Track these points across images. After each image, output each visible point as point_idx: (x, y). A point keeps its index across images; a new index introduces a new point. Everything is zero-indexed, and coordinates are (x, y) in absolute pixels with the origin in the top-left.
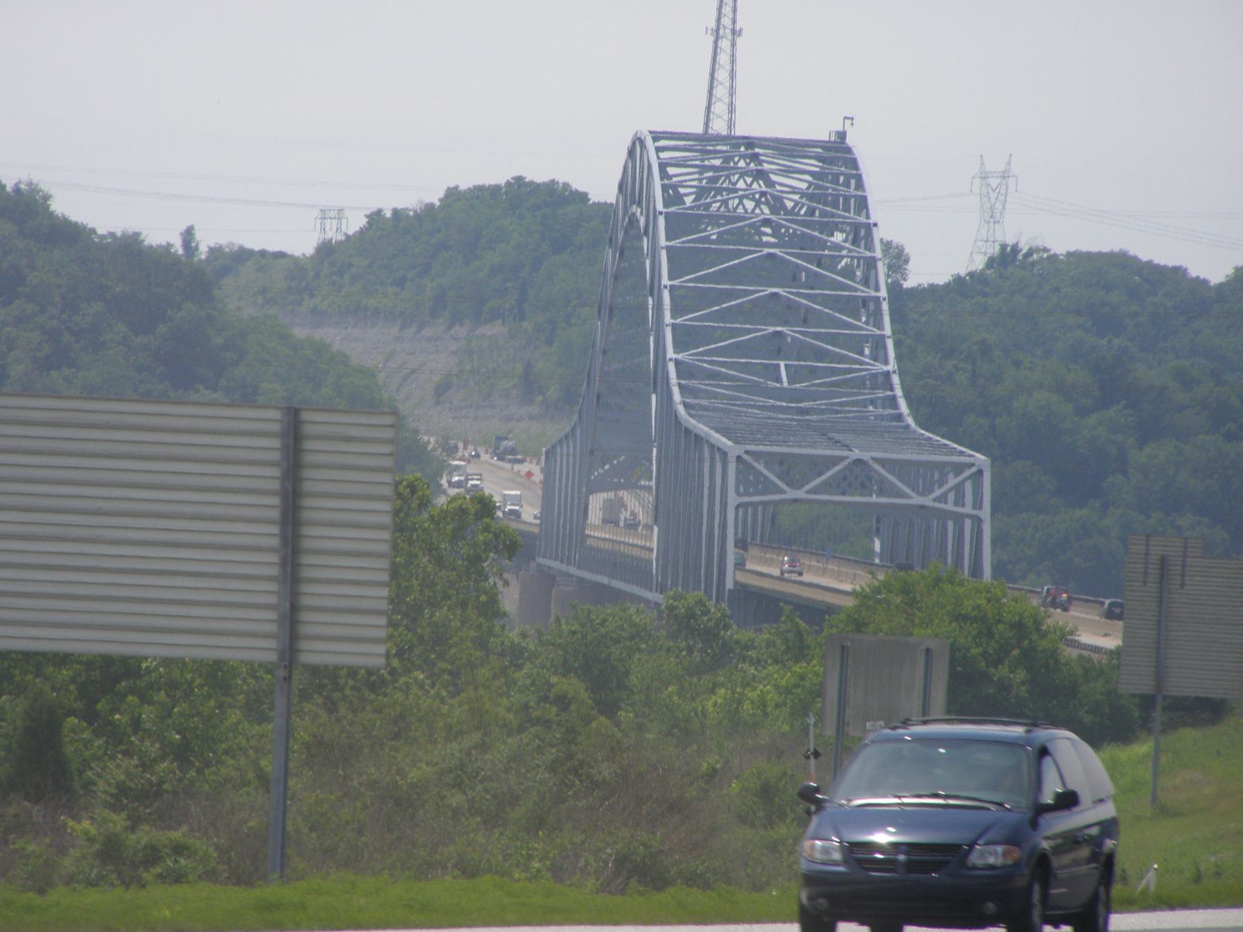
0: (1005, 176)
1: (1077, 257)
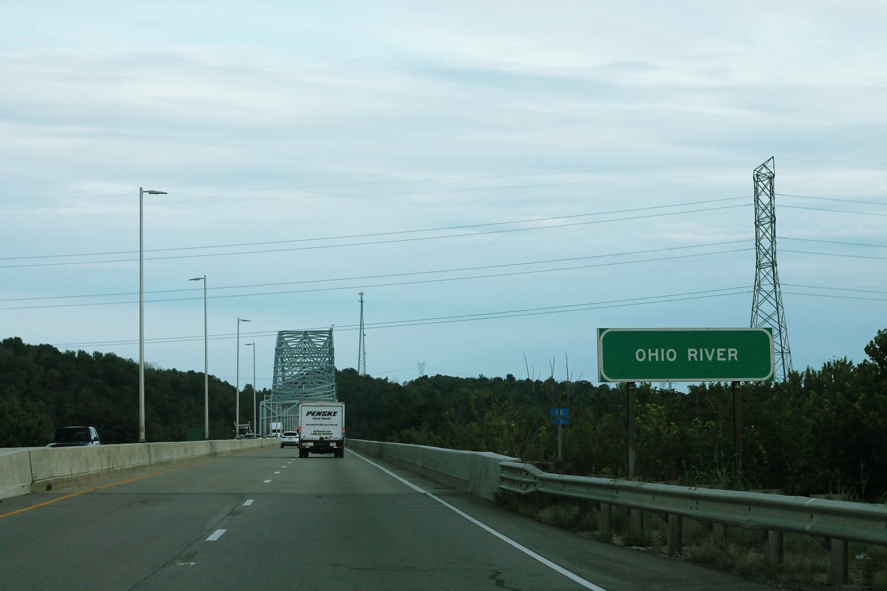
0: (423, 364)
1: (446, 376)
